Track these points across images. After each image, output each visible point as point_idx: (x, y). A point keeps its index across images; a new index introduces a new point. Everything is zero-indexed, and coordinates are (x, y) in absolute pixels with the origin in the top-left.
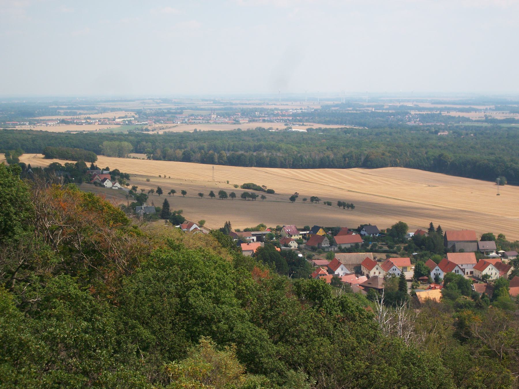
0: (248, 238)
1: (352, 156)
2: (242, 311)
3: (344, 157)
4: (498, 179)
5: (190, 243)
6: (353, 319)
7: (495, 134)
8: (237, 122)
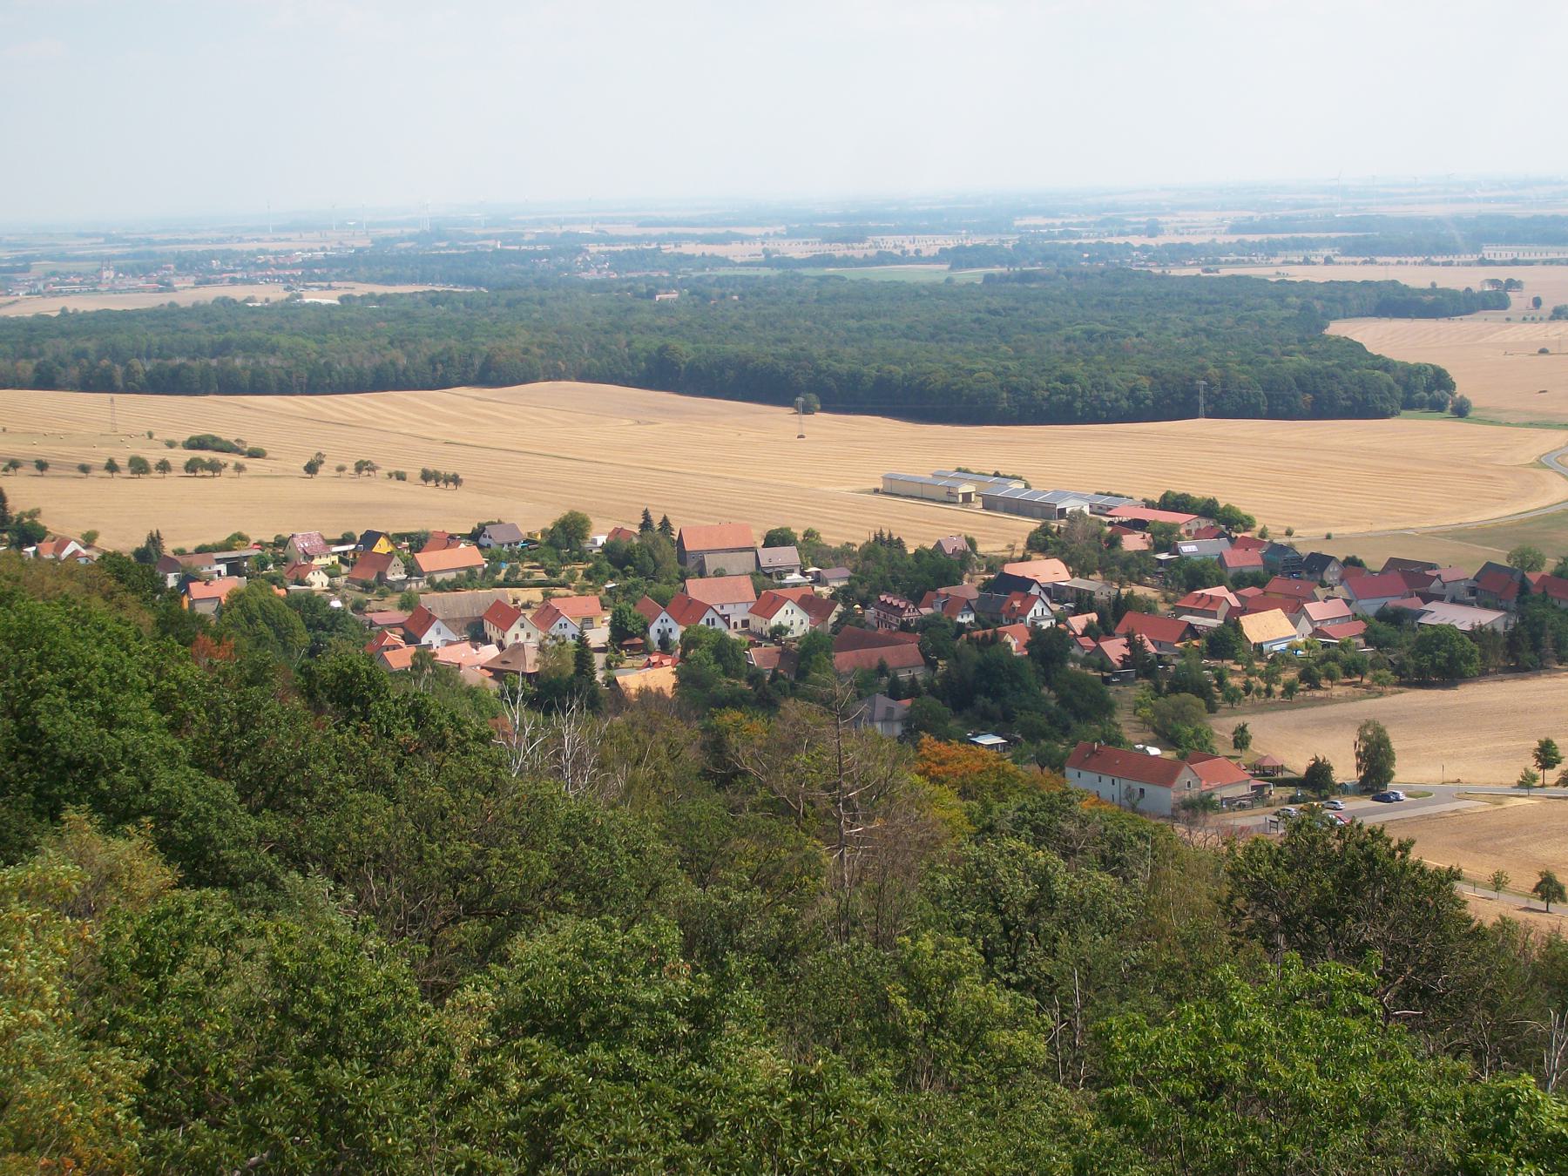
0: (206, 570)
1: (451, 358)
2: (171, 742)
3: (432, 361)
4: (800, 399)
5: (46, 587)
6: (442, 746)
7: (789, 293)
8: (168, 287)
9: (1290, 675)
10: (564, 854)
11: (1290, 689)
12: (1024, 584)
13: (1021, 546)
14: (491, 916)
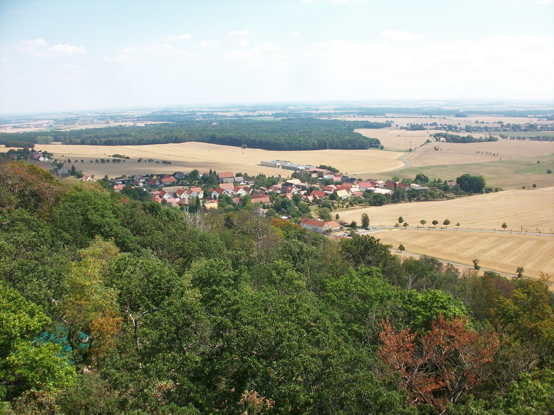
1: (168, 137)
2: (116, 220)
3: (165, 138)
7: (240, 123)
9: (347, 204)
10: (200, 244)
11: (347, 207)
12: (291, 185)
13: (290, 176)
14: (185, 257)
